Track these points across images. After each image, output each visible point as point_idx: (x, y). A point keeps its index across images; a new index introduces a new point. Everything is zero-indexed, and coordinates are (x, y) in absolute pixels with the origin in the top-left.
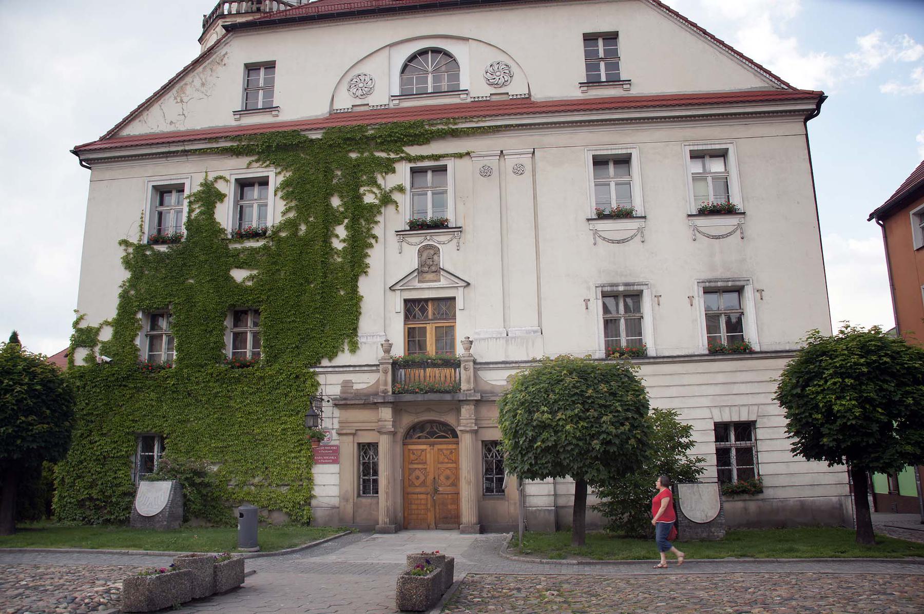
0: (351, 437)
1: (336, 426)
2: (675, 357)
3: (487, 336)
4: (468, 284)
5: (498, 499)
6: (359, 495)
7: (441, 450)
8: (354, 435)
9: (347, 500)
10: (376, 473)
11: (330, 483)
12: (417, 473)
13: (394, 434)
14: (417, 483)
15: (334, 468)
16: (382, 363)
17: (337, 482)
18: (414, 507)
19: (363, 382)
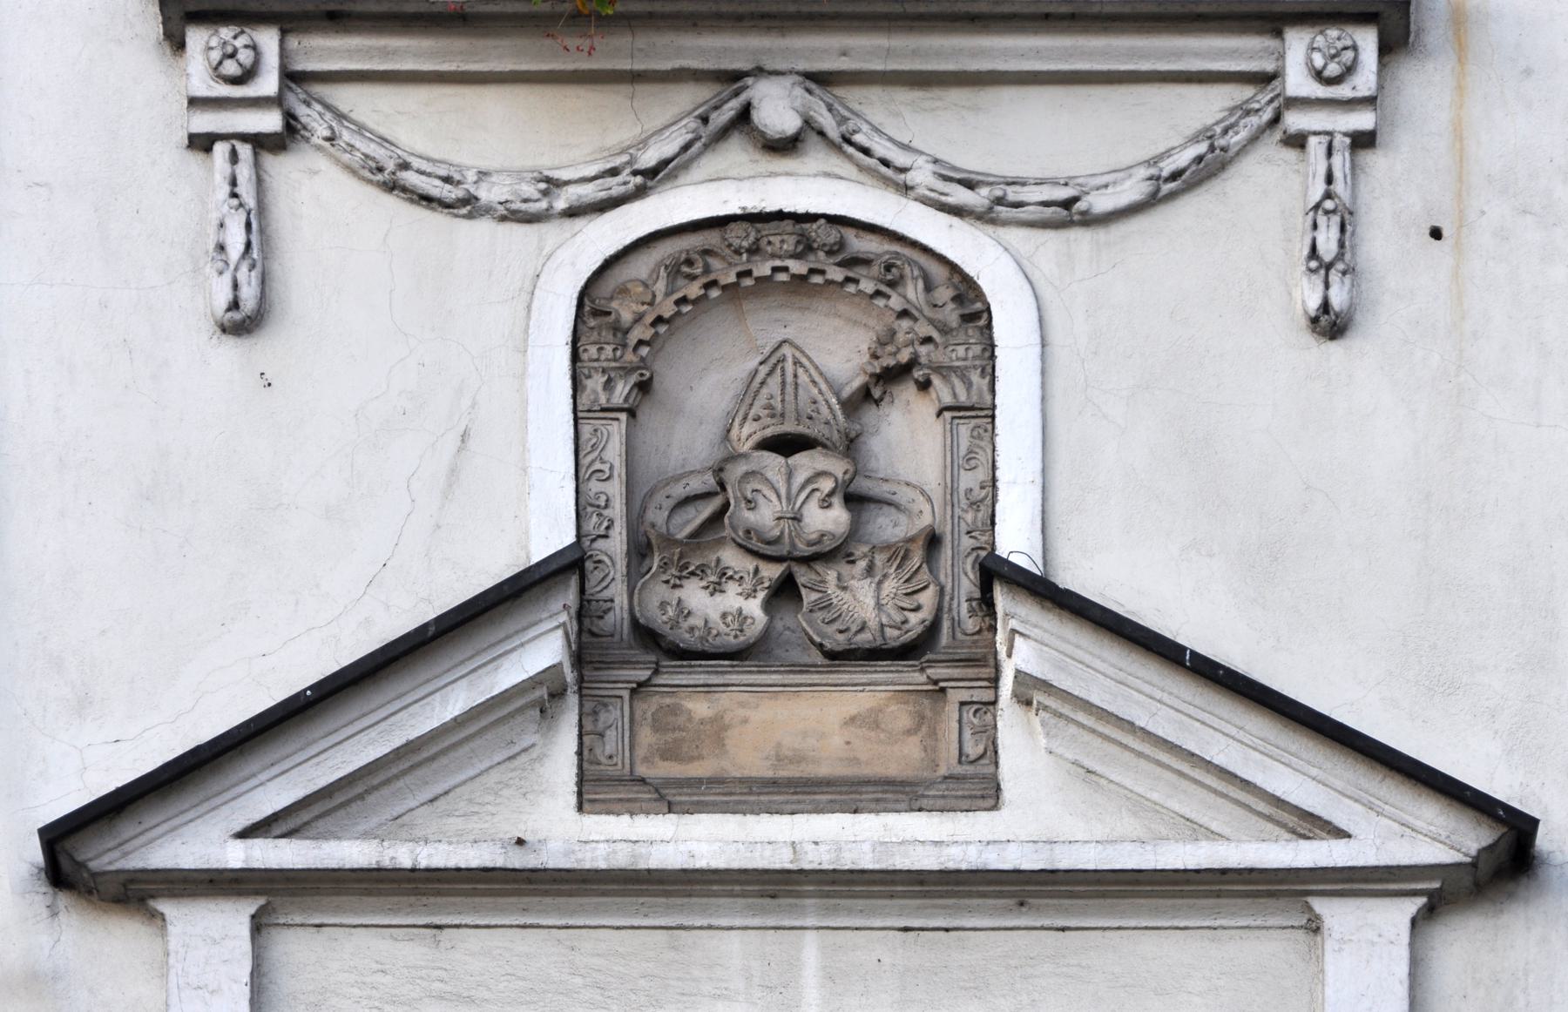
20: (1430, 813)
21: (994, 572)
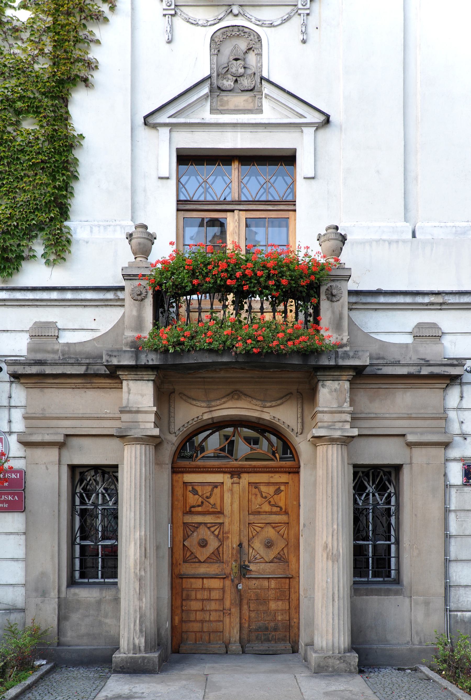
0: (53, 453)
1: (19, 425)
3: (395, 237)
6: (72, 583)
7: (255, 485)
8: (61, 445)
9: (44, 594)
10: (112, 532)
12: (203, 533)
13: (156, 442)
14: (203, 554)
17: (20, 553)
18: (195, 605)
19: (84, 328)
20: (317, 114)
21: (262, 78)
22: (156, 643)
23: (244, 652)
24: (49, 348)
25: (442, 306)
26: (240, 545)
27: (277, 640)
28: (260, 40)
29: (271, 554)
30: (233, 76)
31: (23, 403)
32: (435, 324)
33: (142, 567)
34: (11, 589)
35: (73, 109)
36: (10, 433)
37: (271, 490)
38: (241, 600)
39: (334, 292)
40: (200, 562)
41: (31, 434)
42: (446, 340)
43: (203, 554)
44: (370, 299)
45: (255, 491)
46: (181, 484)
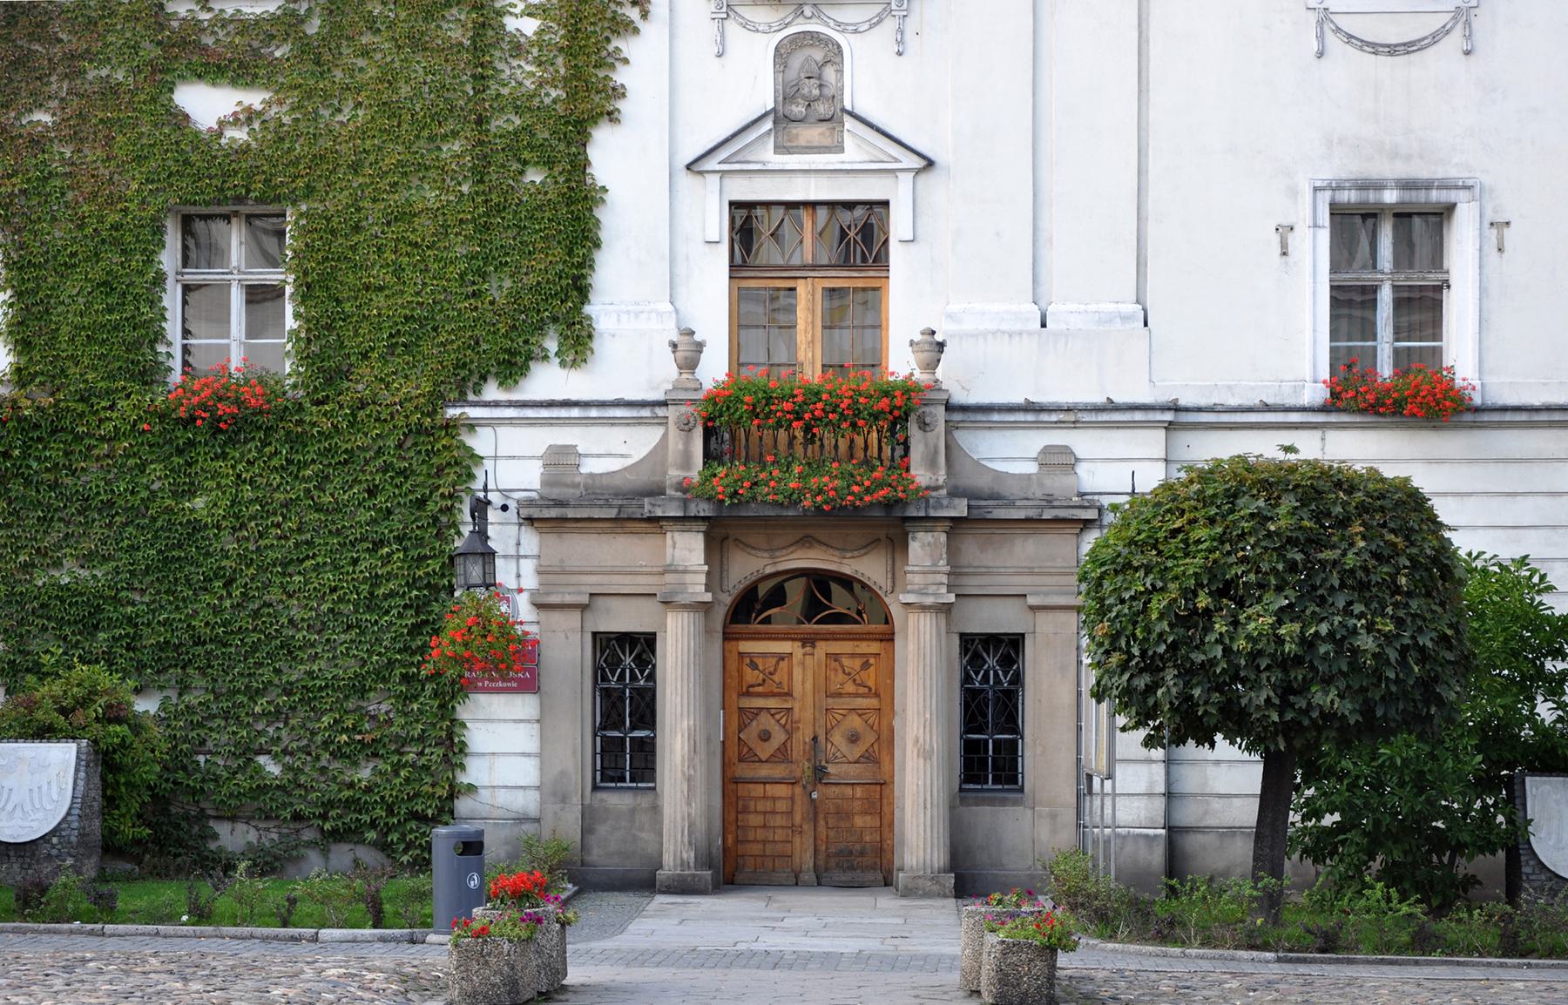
0: (577, 615)
1: (530, 581)
2: (1537, 410)
3: (1018, 327)
4: (930, 164)
5: (1003, 802)
6: (595, 788)
7: (836, 657)
11: (511, 754)
12: (765, 721)
14: (765, 751)
15: (524, 705)
16: (677, 402)
17: (533, 746)
18: (755, 820)
19: (612, 453)
20: (915, 157)
21: (843, 110)
22: (705, 860)
23: (819, 884)
24: (568, 480)
25: (1075, 425)
26: (815, 739)
27: (864, 869)
28: (840, 52)
29: (858, 751)
30: (806, 102)
31: (535, 552)
32: (1066, 447)
33: (691, 765)
34: (521, 792)
35: (593, 153)
36: (520, 591)
37: (857, 663)
38: (816, 814)
39: (928, 420)
40: (760, 761)
41: (548, 594)
42: (1081, 469)
43: (765, 751)
44: (980, 417)
45: (834, 664)
46: (735, 655)
